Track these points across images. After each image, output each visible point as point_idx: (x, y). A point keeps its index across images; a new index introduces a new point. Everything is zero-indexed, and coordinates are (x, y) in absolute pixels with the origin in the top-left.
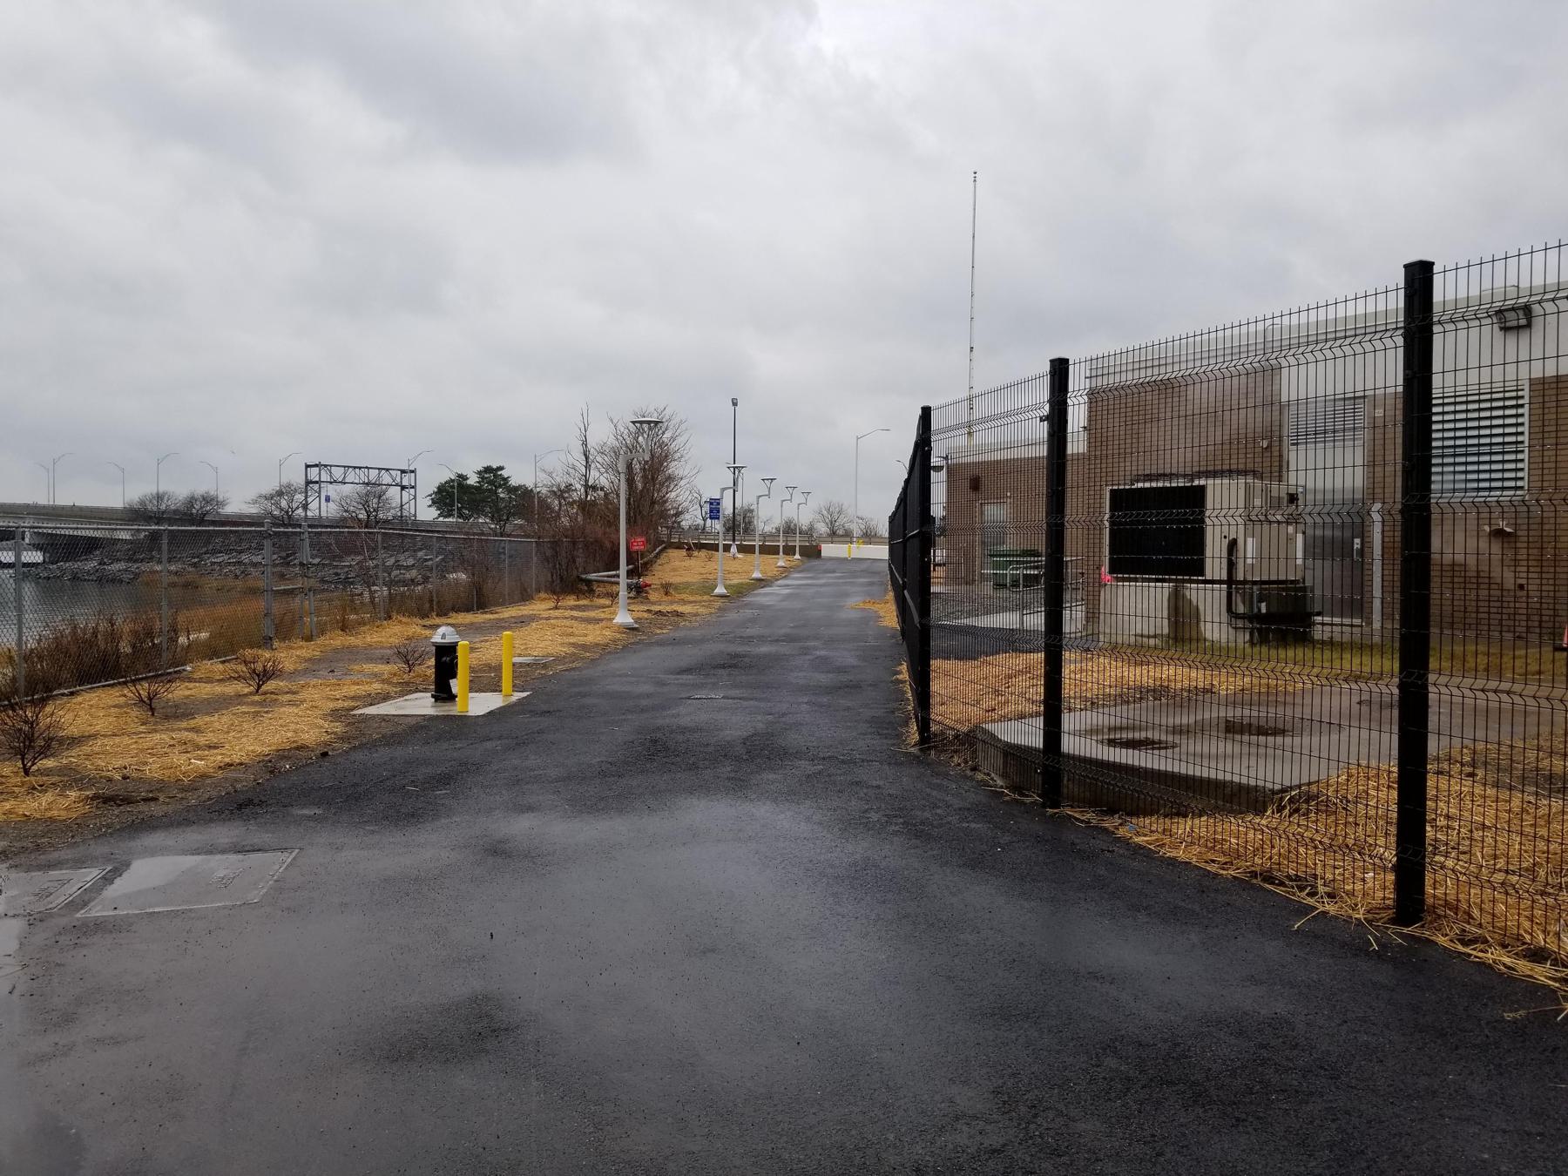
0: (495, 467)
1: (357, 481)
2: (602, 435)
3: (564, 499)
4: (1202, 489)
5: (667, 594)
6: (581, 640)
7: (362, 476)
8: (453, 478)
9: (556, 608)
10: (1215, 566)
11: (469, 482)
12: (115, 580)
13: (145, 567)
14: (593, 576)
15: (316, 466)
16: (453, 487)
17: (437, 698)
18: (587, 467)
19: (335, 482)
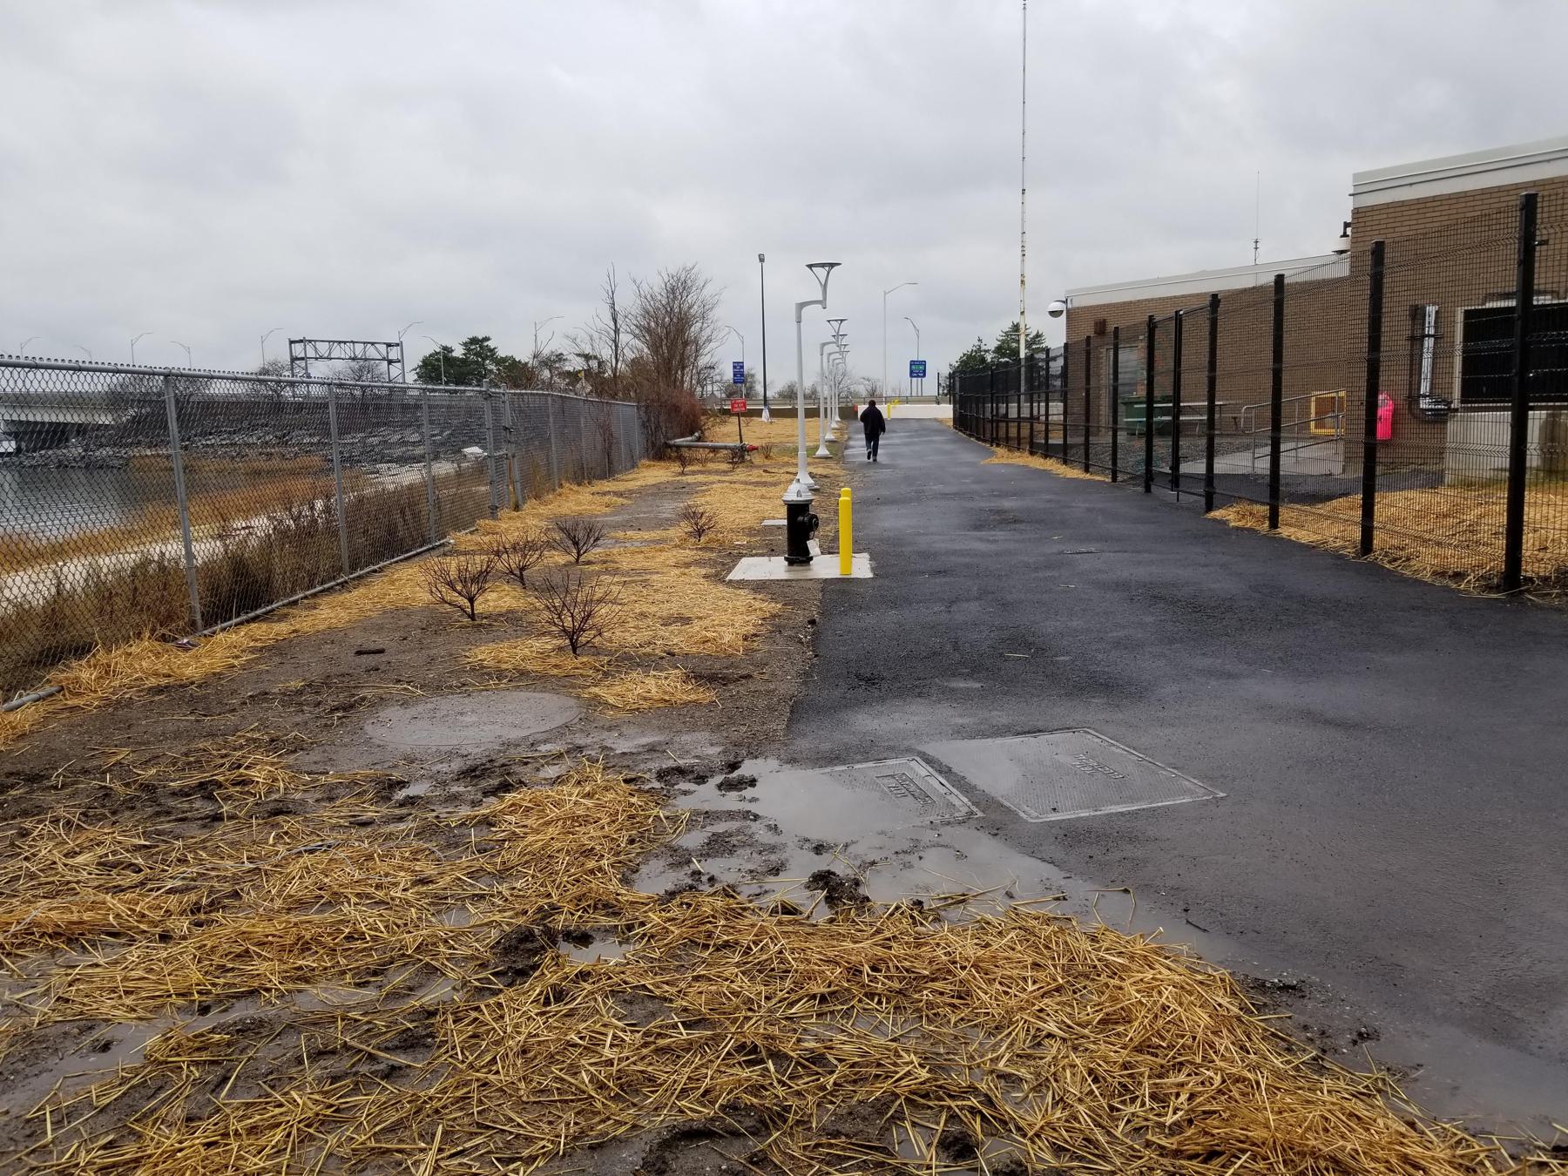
0: (480, 338)
1: (343, 356)
7: (348, 351)
8: (438, 350)
9: (683, 474)
11: (454, 354)
12: (103, 466)
13: (135, 452)
14: (679, 441)
15: (301, 341)
16: (438, 360)
17: (791, 562)
19: (321, 357)
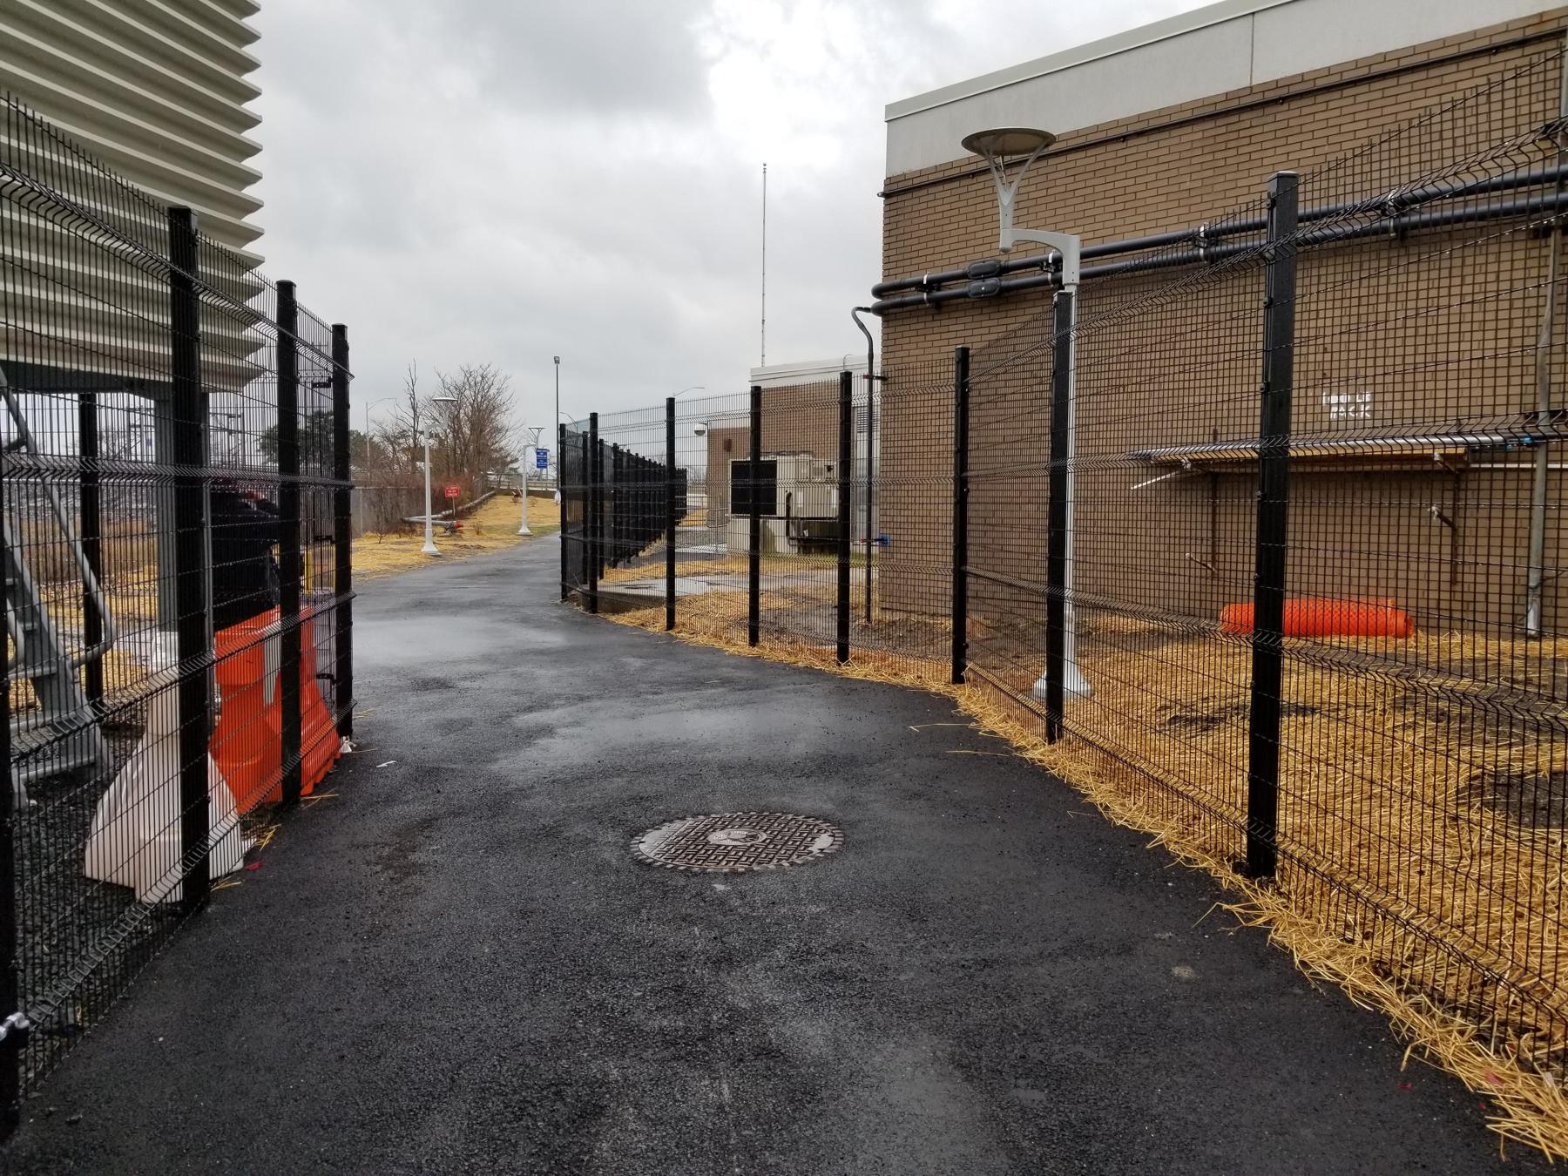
2: (429, 388)
3: (399, 444)
4: (775, 462)
5: (478, 533)
6: (394, 562)
10: (781, 510)
18: (416, 418)
